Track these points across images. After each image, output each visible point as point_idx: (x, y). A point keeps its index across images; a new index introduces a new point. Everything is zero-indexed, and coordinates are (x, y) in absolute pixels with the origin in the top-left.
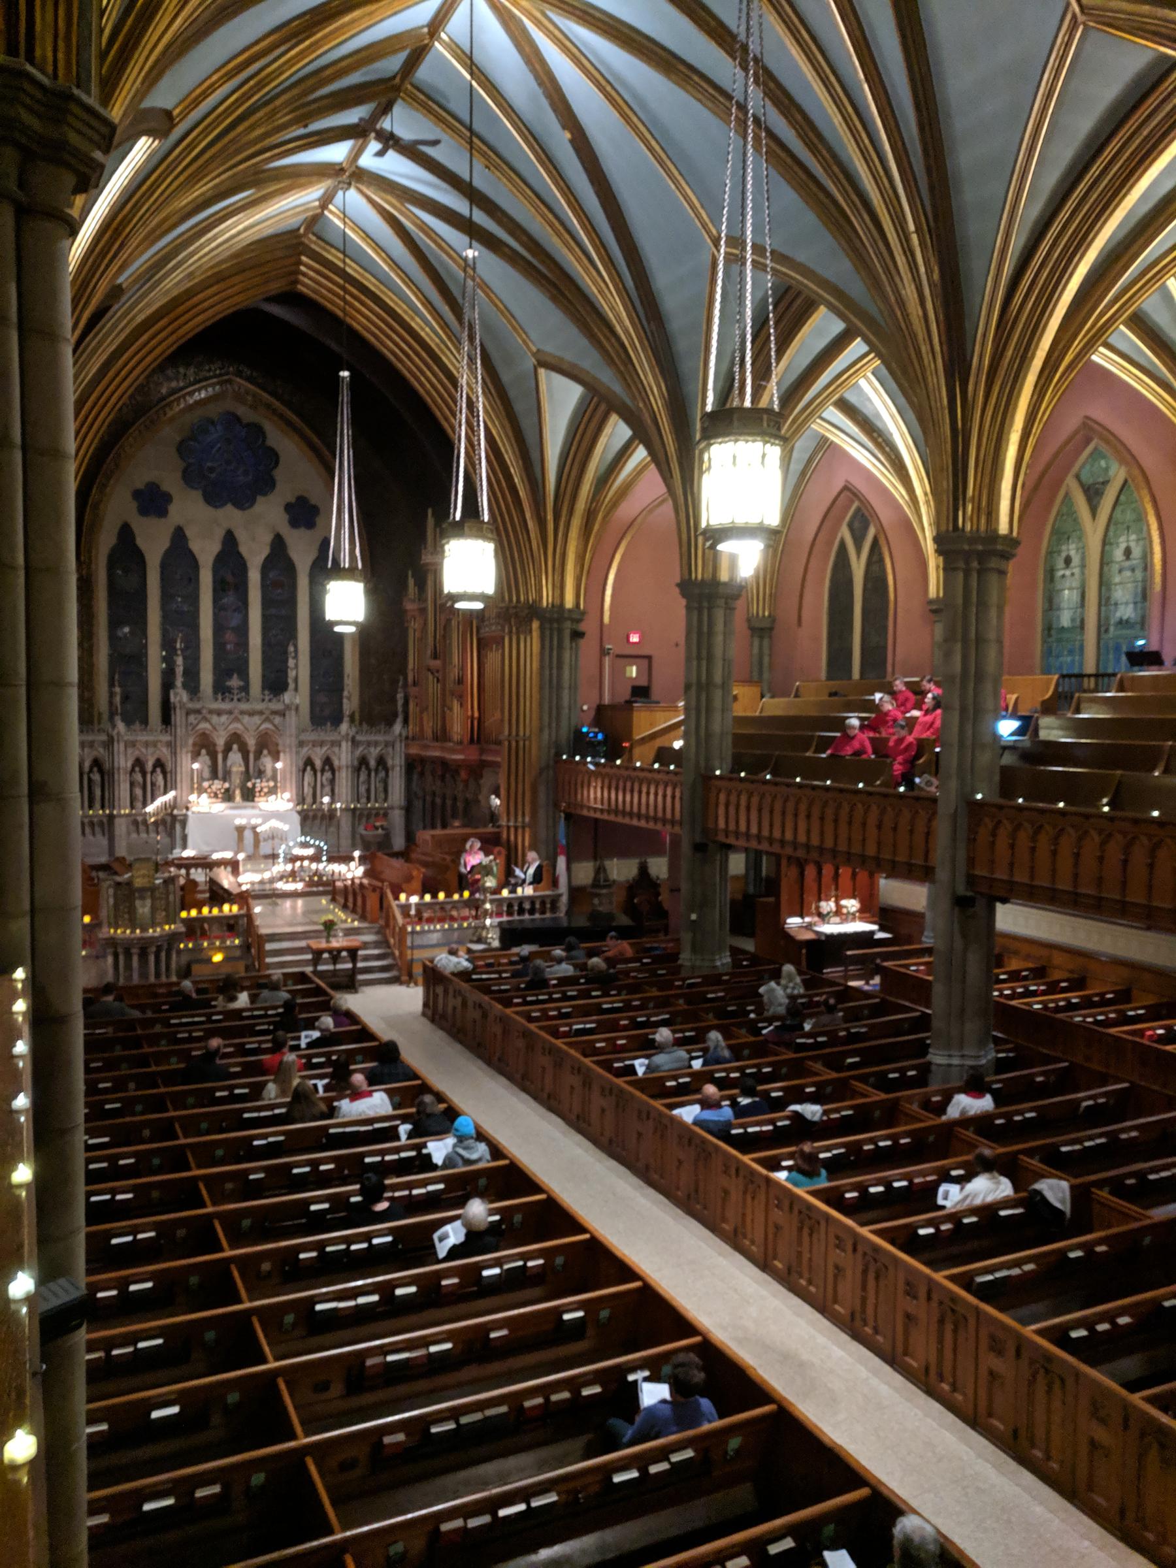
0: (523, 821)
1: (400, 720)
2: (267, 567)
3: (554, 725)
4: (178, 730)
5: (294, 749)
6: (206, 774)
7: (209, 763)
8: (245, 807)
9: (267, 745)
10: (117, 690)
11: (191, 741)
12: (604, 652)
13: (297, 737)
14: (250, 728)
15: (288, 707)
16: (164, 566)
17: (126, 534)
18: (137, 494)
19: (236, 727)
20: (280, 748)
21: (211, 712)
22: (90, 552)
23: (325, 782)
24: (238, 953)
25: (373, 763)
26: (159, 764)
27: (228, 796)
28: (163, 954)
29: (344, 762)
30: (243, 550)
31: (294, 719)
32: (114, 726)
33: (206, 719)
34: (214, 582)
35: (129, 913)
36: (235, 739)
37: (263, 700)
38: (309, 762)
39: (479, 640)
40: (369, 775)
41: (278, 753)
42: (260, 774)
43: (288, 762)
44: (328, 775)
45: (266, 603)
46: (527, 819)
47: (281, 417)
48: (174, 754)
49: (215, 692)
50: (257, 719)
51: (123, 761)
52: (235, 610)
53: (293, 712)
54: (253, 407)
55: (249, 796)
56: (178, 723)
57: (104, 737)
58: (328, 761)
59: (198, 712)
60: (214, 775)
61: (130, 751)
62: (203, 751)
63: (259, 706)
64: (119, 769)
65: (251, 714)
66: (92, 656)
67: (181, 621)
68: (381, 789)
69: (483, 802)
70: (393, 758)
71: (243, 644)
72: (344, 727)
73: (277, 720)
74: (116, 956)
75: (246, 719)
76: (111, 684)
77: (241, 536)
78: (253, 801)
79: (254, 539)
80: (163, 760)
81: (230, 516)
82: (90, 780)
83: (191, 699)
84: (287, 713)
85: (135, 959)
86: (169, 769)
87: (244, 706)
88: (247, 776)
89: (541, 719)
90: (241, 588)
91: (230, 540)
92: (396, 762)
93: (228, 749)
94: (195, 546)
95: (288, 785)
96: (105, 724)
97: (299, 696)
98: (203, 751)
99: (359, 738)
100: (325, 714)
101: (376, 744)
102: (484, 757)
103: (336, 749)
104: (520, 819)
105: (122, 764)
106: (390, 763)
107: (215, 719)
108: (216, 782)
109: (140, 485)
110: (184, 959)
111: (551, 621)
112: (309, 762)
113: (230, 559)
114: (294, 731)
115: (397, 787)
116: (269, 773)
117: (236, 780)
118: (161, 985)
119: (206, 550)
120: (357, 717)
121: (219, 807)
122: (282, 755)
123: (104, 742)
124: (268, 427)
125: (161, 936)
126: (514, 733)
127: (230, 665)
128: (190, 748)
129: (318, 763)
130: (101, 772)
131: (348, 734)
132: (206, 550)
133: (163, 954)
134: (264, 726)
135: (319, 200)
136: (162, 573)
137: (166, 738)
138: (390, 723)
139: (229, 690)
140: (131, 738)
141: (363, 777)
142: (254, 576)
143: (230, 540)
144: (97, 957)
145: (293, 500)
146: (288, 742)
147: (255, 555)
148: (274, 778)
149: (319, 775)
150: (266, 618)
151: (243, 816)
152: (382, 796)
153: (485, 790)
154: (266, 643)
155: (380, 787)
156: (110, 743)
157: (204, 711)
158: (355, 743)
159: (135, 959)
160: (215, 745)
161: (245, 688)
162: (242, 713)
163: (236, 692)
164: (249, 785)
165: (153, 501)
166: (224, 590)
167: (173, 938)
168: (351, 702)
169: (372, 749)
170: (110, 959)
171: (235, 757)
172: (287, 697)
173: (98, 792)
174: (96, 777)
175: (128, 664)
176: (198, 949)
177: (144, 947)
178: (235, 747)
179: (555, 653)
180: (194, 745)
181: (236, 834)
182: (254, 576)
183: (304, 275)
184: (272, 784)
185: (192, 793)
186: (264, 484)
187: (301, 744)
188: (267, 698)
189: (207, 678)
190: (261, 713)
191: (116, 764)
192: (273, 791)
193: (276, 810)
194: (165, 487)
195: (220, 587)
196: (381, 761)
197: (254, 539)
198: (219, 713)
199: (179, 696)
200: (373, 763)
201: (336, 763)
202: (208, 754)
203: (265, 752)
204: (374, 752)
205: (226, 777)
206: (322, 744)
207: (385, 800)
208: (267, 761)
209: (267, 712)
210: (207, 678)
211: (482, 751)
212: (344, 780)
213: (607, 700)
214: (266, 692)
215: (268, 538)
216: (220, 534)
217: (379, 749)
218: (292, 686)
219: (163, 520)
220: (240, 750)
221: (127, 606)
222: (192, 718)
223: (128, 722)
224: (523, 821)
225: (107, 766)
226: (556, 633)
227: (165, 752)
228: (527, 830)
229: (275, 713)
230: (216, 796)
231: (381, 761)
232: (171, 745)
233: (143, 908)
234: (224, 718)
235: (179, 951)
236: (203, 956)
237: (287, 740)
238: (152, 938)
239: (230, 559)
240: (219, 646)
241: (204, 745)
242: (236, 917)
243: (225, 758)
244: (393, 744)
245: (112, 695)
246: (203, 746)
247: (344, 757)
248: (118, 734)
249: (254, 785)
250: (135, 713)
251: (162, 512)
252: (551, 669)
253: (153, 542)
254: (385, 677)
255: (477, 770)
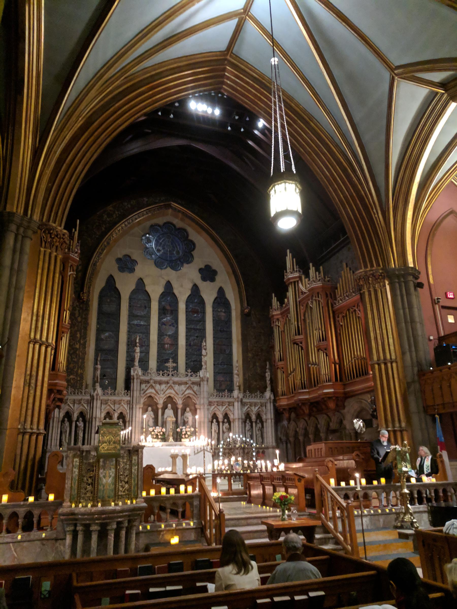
0: (400, 426)
1: (269, 389)
2: (189, 301)
3: (413, 349)
4: (135, 393)
5: (206, 407)
6: (151, 422)
7: (153, 416)
8: (175, 445)
9: (189, 405)
10: (99, 366)
11: (142, 400)
12: (434, 302)
13: (208, 398)
14: (179, 393)
15: (202, 380)
16: (131, 299)
17: (111, 280)
18: (119, 260)
19: (170, 392)
20: (197, 406)
21: (155, 382)
22: (89, 288)
23: (225, 430)
24: (192, 536)
25: (254, 417)
26: (122, 416)
27: (164, 439)
28: (123, 533)
29: (236, 416)
30: (176, 291)
31: (205, 386)
32: (94, 390)
33: (152, 387)
34: (159, 309)
35: (92, 484)
36: (170, 400)
37: (187, 375)
38: (215, 416)
39: (334, 312)
40: (252, 426)
41: (196, 410)
42: (185, 423)
43: (202, 416)
44: (227, 425)
45: (189, 321)
46: (403, 425)
47: (197, 223)
48: (131, 409)
49: (158, 370)
50: (183, 387)
51: (99, 414)
52: (170, 325)
53: (205, 383)
54: (182, 220)
55: (178, 437)
56: (135, 389)
57: (88, 397)
58: (226, 416)
59: (148, 382)
60: (156, 424)
61: (103, 406)
62: (150, 409)
63: (185, 379)
64: (96, 418)
65: (180, 384)
66: (85, 348)
67: (139, 330)
68: (260, 435)
69: (348, 427)
70: (266, 414)
71: (175, 344)
72: (236, 393)
73: (196, 388)
74: (75, 534)
75: (176, 387)
76: (96, 364)
77: (175, 285)
78: (181, 441)
79: (182, 286)
80: (124, 413)
81: (169, 274)
82: (76, 426)
83: (144, 374)
84: (202, 383)
85: (94, 537)
86: (127, 420)
87: (176, 379)
88: (176, 424)
89: (401, 346)
90: (175, 312)
91: (169, 286)
92: (269, 416)
93: (165, 408)
94: (149, 289)
95: (202, 431)
96: (90, 389)
97: (208, 371)
98: (150, 409)
99: (245, 400)
100: (223, 384)
101: (255, 405)
102: (348, 390)
103: (231, 408)
104: (397, 425)
105: (98, 415)
106: (264, 417)
107: (158, 387)
108: (157, 427)
109: (120, 256)
110: (143, 541)
111: (398, 277)
112: (215, 416)
113: (168, 292)
114: (206, 395)
115: (270, 434)
116: (190, 422)
117: (170, 426)
118: (123, 560)
119: (155, 291)
120: (242, 388)
121: (158, 444)
122: (198, 411)
123: (87, 400)
124: (189, 230)
125: (122, 511)
126: (382, 357)
127: (167, 357)
128: (142, 406)
129: (220, 417)
130: (84, 421)
131: (238, 398)
132: (155, 291)
133: (123, 533)
134: (187, 392)
135: (243, 9)
136: (130, 303)
137: (128, 398)
138: (263, 390)
139: (167, 368)
140: (105, 398)
141: (248, 427)
142: (182, 307)
143: (169, 286)
144: (56, 540)
145: (203, 267)
146: (202, 402)
147: (182, 294)
148: (194, 426)
149: (221, 424)
150: (188, 330)
151: (176, 449)
152: (260, 439)
153: (348, 417)
154: (188, 344)
155: (259, 433)
156: (91, 402)
157: (152, 381)
158: (243, 404)
159: (94, 537)
160: (157, 404)
161: (176, 368)
162: (174, 383)
163: (171, 370)
164: (178, 430)
165: (127, 264)
166: (164, 314)
167: (133, 515)
168: (238, 380)
169: (253, 408)
170: (69, 539)
171: (169, 412)
172: (201, 373)
173: (81, 434)
174: (81, 424)
175: (107, 354)
176: (156, 532)
177: (104, 522)
178: (169, 406)
179: (405, 297)
180: (144, 404)
181: (171, 460)
182: (182, 307)
183: (228, 78)
184: (193, 429)
185: (142, 433)
186: (187, 258)
187: (210, 404)
188: (189, 374)
189: (153, 363)
190: (186, 383)
191: (94, 416)
192: (194, 433)
193: (197, 443)
194: (134, 257)
195: (162, 311)
196: (259, 416)
197: (182, 286)
198: (160, 383)
199: (137, 371)
200: (254, 417)
201: (231, 417)
202: (153, 410)
203: (188, 409)
204: (255, 410)
205: (164, 424)
206: (222, 404)
207: (263, 443)
208: (189, 415)
209: (190, 382)
210: (153, 363)
211: (345, 385)
212: (237, 425)
213: (442, 334)
214: (189, 371)
215: (190, 286)
216: (163, 283)
217: (257, 408)
218: (204, 367)
219: (132, 274)
220: (172, 408)
221: (109, 320)
222: (143, 386)
223: (104, 387)
224: (400, 426)
225: (88, 416)
226: (403, 284)
227: (125, 408)
228: (405, 433)
229: (193, 383)
230: (157, 437)
231: (259, 416)
232: (130, 404)
233: (107, 478)
234: (163, 386)
235: (138, 533)
236: (160, 539)
237: (201, 401)
238: (114, 512)
239: (168, 292)
240: (161, 345)
241: (151, 404)
242: (191, 497)
243: (163, 414)
244: (264, 405)
245: (95, 369)
246: (149, 406)
247: (236, 413)
248: (97, 395)
249: (182, 429)
250: (107, 380)
251: (132, 270)
252: (404, 309)
253: (126, 286)
254: (258, 364)
255: (342, 399)
